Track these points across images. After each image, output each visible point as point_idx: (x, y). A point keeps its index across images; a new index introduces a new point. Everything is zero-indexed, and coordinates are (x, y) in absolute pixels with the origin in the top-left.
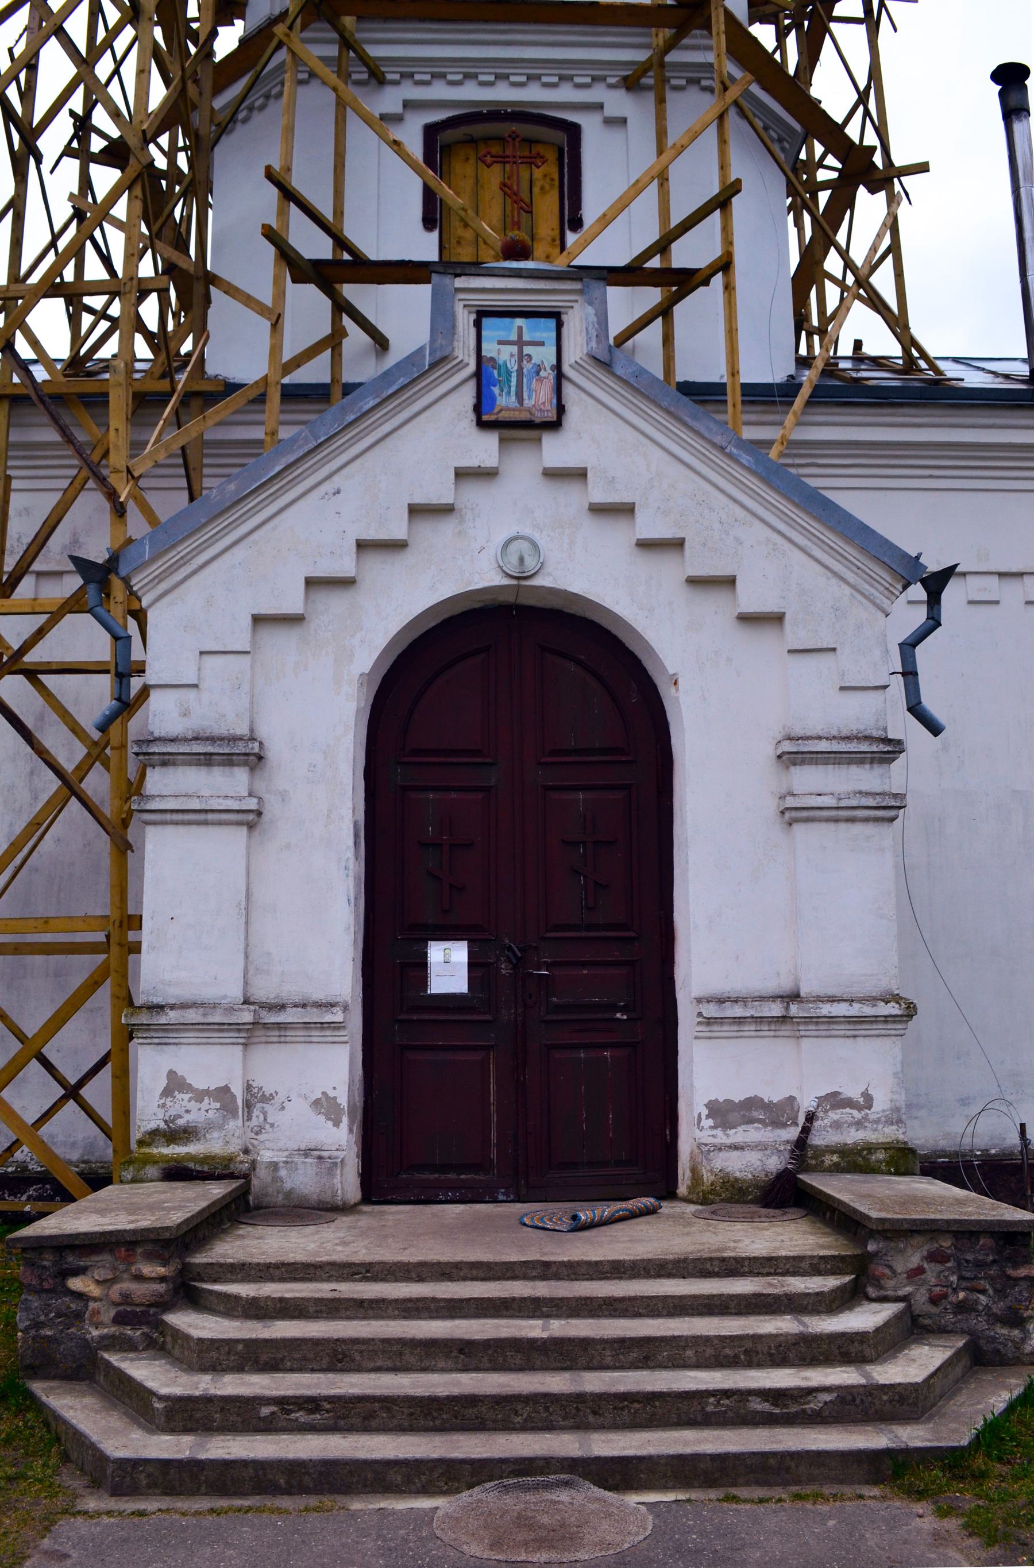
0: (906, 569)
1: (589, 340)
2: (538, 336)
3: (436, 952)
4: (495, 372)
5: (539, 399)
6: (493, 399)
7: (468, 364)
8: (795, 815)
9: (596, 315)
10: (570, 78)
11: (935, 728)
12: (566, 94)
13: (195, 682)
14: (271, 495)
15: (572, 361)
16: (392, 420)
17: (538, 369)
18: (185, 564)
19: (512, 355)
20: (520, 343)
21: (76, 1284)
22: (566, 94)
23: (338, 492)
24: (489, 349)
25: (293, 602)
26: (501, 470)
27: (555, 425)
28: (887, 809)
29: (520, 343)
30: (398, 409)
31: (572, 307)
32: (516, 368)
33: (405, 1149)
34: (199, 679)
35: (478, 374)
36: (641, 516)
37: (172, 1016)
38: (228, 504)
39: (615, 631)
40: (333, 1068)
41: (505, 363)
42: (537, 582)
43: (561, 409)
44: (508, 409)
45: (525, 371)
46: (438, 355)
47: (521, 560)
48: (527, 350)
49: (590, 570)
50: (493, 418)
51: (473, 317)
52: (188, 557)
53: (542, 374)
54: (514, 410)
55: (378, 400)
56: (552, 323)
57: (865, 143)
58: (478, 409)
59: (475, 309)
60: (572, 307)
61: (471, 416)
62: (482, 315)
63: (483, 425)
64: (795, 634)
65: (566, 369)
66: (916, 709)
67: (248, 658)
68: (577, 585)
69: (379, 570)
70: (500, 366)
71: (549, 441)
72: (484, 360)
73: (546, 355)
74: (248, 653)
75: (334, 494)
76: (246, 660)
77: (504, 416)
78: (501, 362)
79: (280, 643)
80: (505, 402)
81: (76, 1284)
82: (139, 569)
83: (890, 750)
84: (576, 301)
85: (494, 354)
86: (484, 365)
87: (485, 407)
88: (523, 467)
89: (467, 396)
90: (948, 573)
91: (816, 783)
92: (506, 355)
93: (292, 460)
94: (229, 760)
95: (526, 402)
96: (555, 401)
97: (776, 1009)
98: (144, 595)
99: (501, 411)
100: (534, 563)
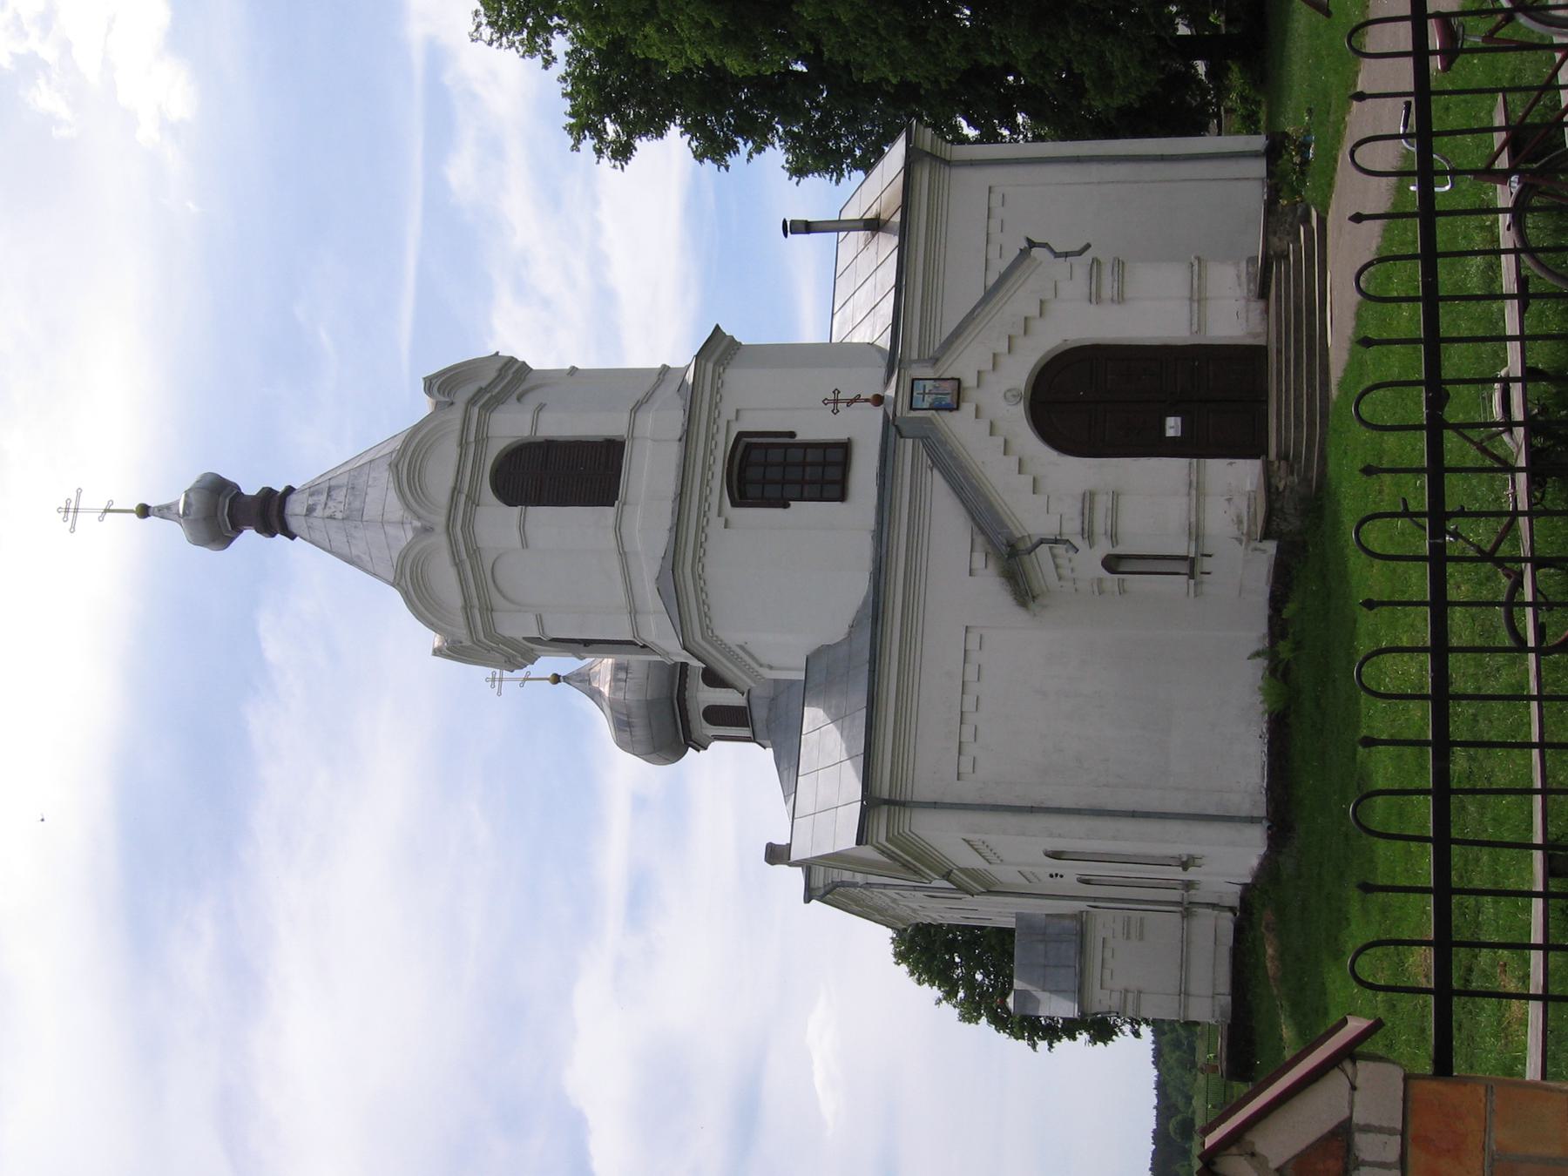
0: (1024, 254)
3: (1170, 433)
5: (948, 387)
8: (1120, 298)
11: (1088, 246)
12: (721, 438)
20: (924, 393)
21: (1281, 487)
22: (721, 438)
24: (926, 405)
28: (1119, 264)
29: (924, 393)
35: (937, 409)
36: (998, 351)
37: (1193, 519)
40: (1217, 469)
49: (1019, 372)
57: (1410, 48)
58: (951, 410)
61: (955, 413)
62: (911, 408)
64: (1049, 295)
66: (1080, 253)
68: (1025, 377)
71: (965, 384)
73: (929, 385)
80: (948, 399)
81: (1281, 487)
83: (1096, 262)
90: (1028, 240)
91: (1108, 290)
92: (929, 399)
94: (1092, 502)
97: (1195, 305)
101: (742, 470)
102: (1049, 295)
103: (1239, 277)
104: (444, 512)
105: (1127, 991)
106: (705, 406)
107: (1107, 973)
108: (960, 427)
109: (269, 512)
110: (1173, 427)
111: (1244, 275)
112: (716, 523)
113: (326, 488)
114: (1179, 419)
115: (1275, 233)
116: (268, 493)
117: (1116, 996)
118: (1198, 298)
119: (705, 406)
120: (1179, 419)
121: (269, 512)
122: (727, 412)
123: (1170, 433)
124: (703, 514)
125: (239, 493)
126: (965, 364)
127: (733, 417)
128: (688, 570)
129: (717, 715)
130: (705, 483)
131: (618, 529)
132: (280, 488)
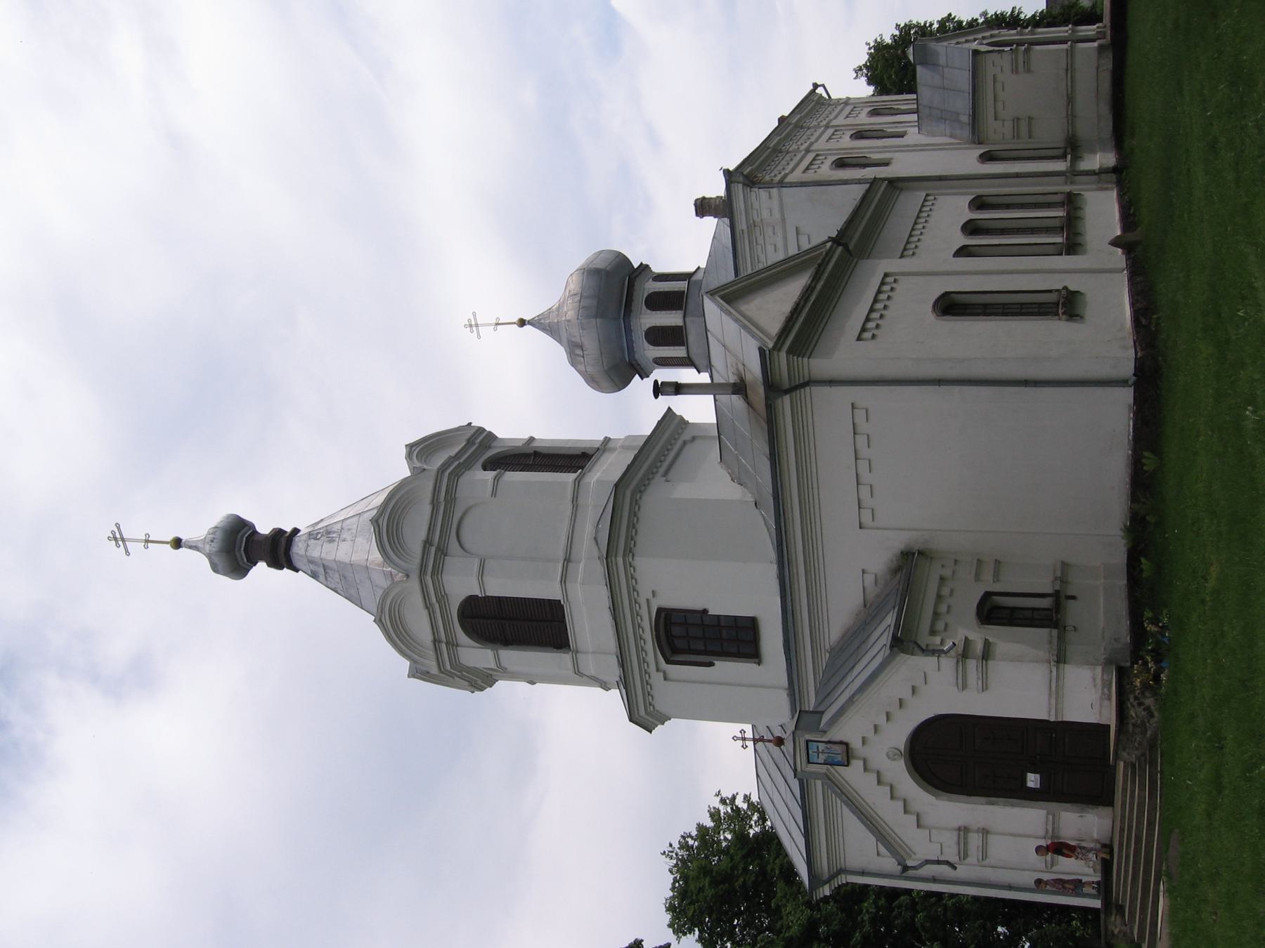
3: (1030, 784)
12: (644, 612)
22: (644, 612)
33: (1095, 792)
35: (831, 764)
43: (841, 743)
64: (919, 682)
80: (839, 758)
81: (1116, 932)
92: (822, 758)
101: (667, 632)
102: (919, 682)
103: (1094, 680)
104: (432, 653)
105: (1018, 119)
106: (626, 514)
107: (1000, 105)
108: (852, 775)
109: (280, 550)
110: (1033, 780)
111: (1099, 681)
112: (657, 678)
113: (324, 533)
114: (1038, 776)
115: (1124, 749)
116: (278, 533)
117: (1009, 124)
118: (1057, 692)
119: (626, 514)
120: (1038, 776)
121: (280, 550)
122: (645, 593)
123: (1030, 784)
124: (644, 673)
125: (255, 532)
126: (850, 730)
127: (650, 596)
128: (628, 493)
129: (659, 336)
130: (640, 650)
131: (577, 482)
132: (288, 529)
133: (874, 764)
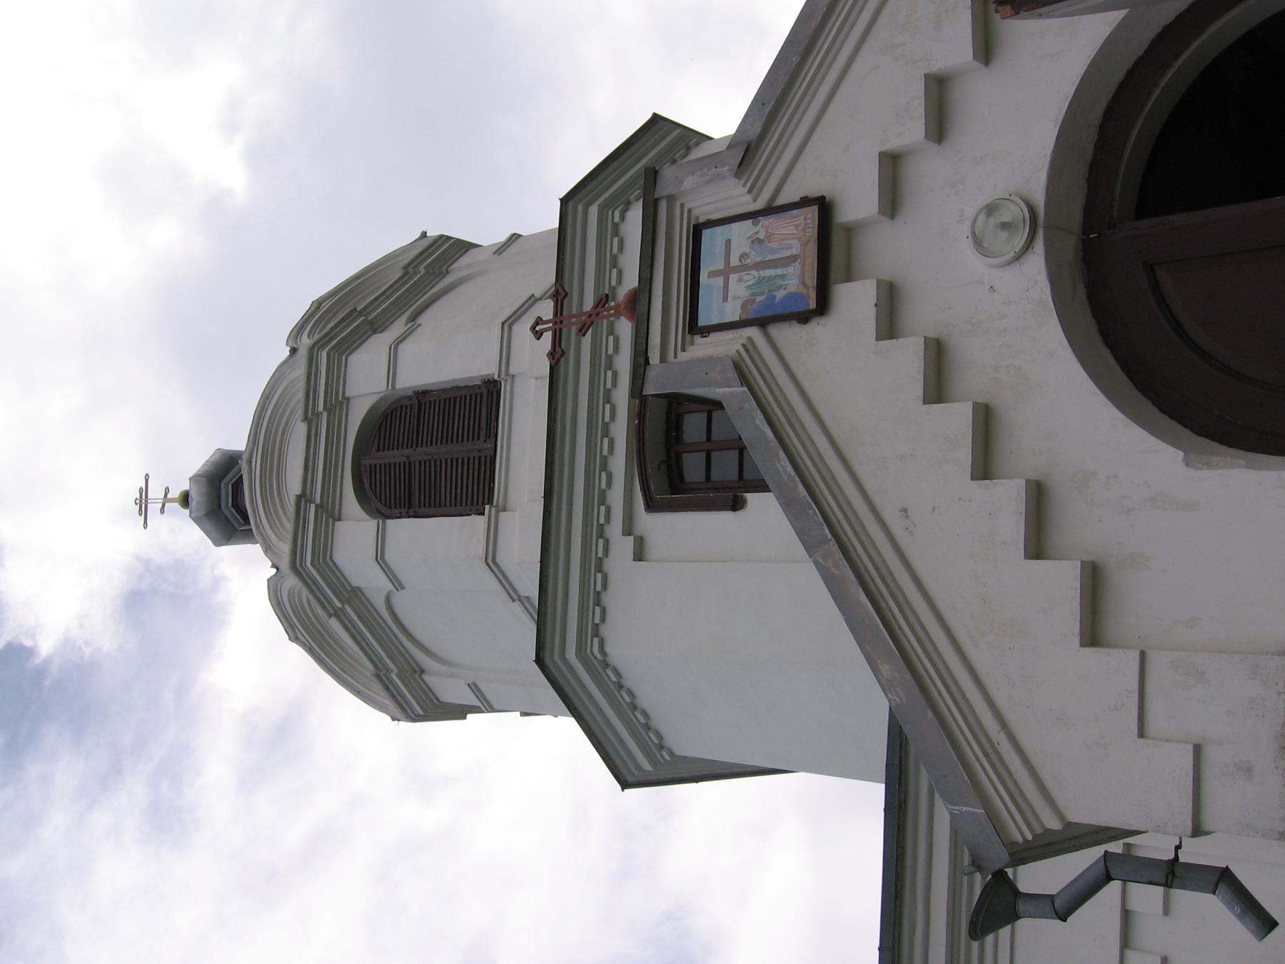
1: (721, 177)
2: (720, 250)
4: (759, 299)
5: (795, 233)
6: (790, 297)
7: (750, 339)
9: (693, 174)
10: (601, 528)
13: (1190, 748)
14: (901, 611)
15: (748, 198)
16: (814, 437)
17: (756, 242)
18: (997, 752)
19: (740, 280)
20: (726, 273)
23: (905, 510)
25: (1061, 579)
26: (887, 277)
27: (824, 207)
29: (726, 273)
30: (798, 427)
31: (690, 211)
32: (754, 272)
34: (1187, 742)
35: (763, 323)
38: (909, 677)
39: (1120, 75)
41: (749, 288)
42: (1039, 199)
43: (805, 202)
44: (802, 275)
45: (758, 260)
46: (733, 375)
47: (1005, 226)
48: (734, 261)
50: (813, 295)
51: (698, 339)
52: (987, 745)
53: (762, 236)
54: (803, 266)
55: (782, 454)
56: (706, 234)
58: (804, 318)
59: (688, 336)
60: (690, 211)
62: (694, 327)
63: (823, 306)
65: (760, 204)
67: (1151, 655)
68: (1045, 137)
69: (1025, 449)
70: (753, 294)
72: (744, 317)
74: (1143, 655)
75: (907, 517)
76: (1160, 664)
77: (812, 281)
78: (747, 294)
79: (1141, 603)
82: (998, 828)
84: (682, 206)
85: (738, 304)
86: (750, 316)
87: (800, 308)
88: (888, 249)
89: (788, 334)
92: (739, 288)
93: (853, 577)
95: (794, 251)
96: (795, 212)
98: (1042, 824)
99: (804, 284)
100: (1013, 207)
133: (924, 316)
